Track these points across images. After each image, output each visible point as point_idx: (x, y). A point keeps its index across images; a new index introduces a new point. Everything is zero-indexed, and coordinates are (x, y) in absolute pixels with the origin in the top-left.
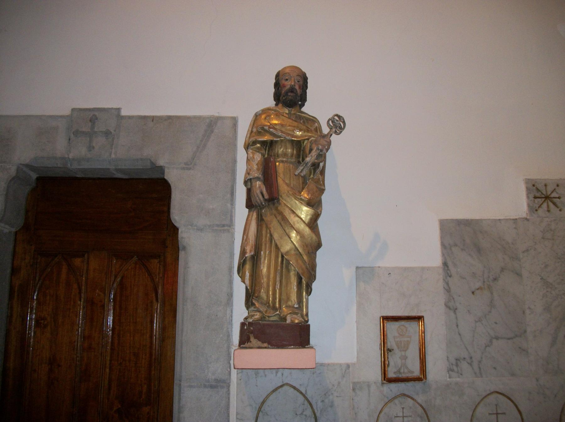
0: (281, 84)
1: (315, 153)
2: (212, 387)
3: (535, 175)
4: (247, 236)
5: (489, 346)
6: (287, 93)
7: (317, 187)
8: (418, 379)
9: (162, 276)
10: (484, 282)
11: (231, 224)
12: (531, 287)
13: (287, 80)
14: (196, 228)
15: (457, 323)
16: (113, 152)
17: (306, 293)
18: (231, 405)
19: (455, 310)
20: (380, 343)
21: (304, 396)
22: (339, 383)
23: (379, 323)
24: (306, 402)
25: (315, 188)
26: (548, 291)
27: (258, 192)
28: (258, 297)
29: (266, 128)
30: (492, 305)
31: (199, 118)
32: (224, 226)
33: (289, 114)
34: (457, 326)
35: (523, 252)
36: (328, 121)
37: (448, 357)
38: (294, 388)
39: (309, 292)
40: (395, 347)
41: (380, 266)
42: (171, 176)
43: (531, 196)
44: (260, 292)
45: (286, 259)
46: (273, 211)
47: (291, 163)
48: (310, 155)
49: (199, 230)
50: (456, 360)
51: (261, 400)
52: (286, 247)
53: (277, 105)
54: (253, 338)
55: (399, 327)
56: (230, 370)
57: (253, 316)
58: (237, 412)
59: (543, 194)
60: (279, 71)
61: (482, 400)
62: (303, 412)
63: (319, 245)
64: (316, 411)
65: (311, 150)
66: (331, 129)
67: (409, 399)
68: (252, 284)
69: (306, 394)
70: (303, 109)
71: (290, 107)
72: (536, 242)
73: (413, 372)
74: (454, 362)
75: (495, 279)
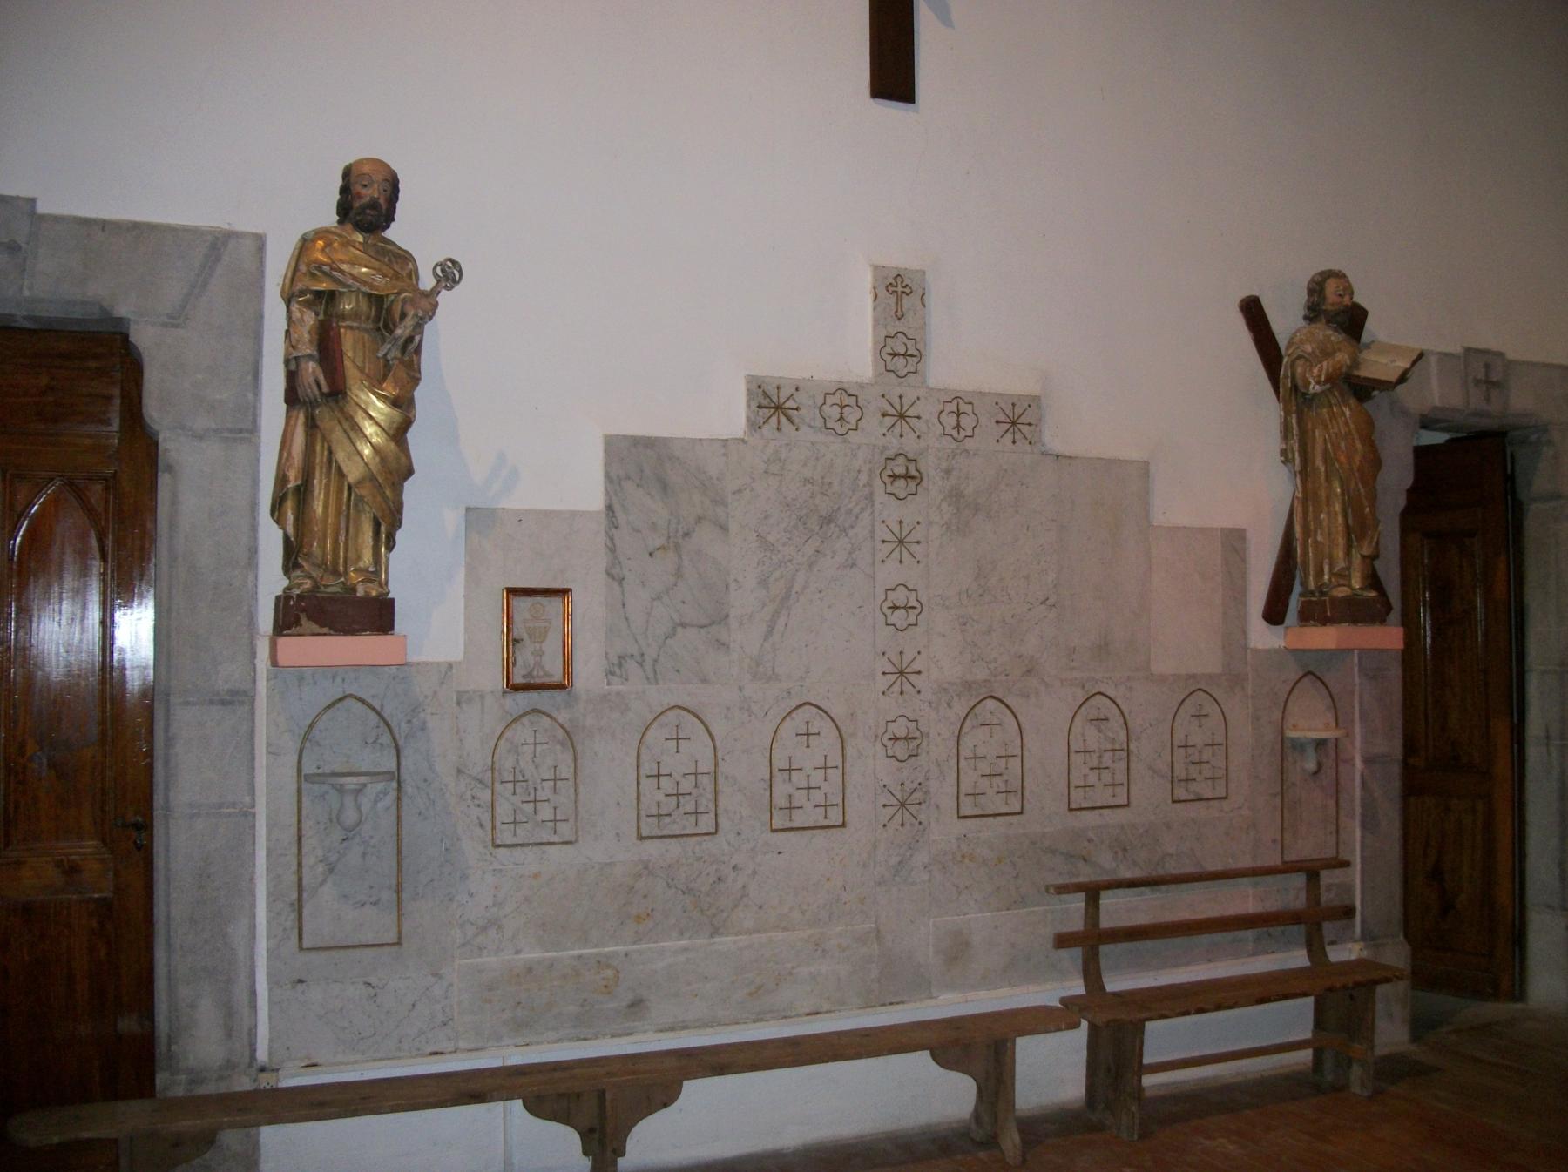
0: (353, 192)
1: (412, 323)
2: (223, 703)
3: (762, 371)
4: (289, 454)
5: (671, 638)
6: (363, 209)
7: (408, 374)
8: (561, 686)
10: (669, 537)
11: (254, 429)
12: (741, 548)
13: (365, 186)
14: (190, 433)
15: (623, 601)
16: (26, 283)
17: (386, 548)
18: (257, 731)
19: (621, 581)
20: (500, 630)
21: (378, 713)
22: (435, 693)
23: (500, 598)
24: (382, 724)
25: (405, 376)
26: (766, 556)
27: (311, 380)
28: (308, 555)
29: (326, 268)
30: (679, 573)
31: (195, 232)
32: (241, 431)
33: (365, 242)
34: (624, 605)
35: (734, 493)
36: (435, 268)
37: (606, 654)
38: (363, 701)
39: (390, 548)
40: (525, 636)
41: (506, 506)
42: (143, 337)
43: (754, 405)
44: (312, 546)
45: (356, 495)
46: (336, 413)
47: (366, 331)
48: (402, 326)
49: (196, 437)
50: (620, 657)
51: (308, 722)
52: (353, 473)
53: (340, 222)
54: (305, 619)
55: (533, 605)
56: (255, 674)
57: (300, 585)
58: (267, 743)
59: (773, 402)
60: (351, 164)
61: (656, 718)
62: (377, 739)
63: (410, 472)
64: (398, 737)
65: (403, 316)
66: (439, 281)
67: (545, 718)
68: (297, 533)
69: (382, 709)
70: (390, 234)
71: (366, 233)
72: (753, 479)
73: (551, 676)
74: (616, 661)
75: (686, 535)
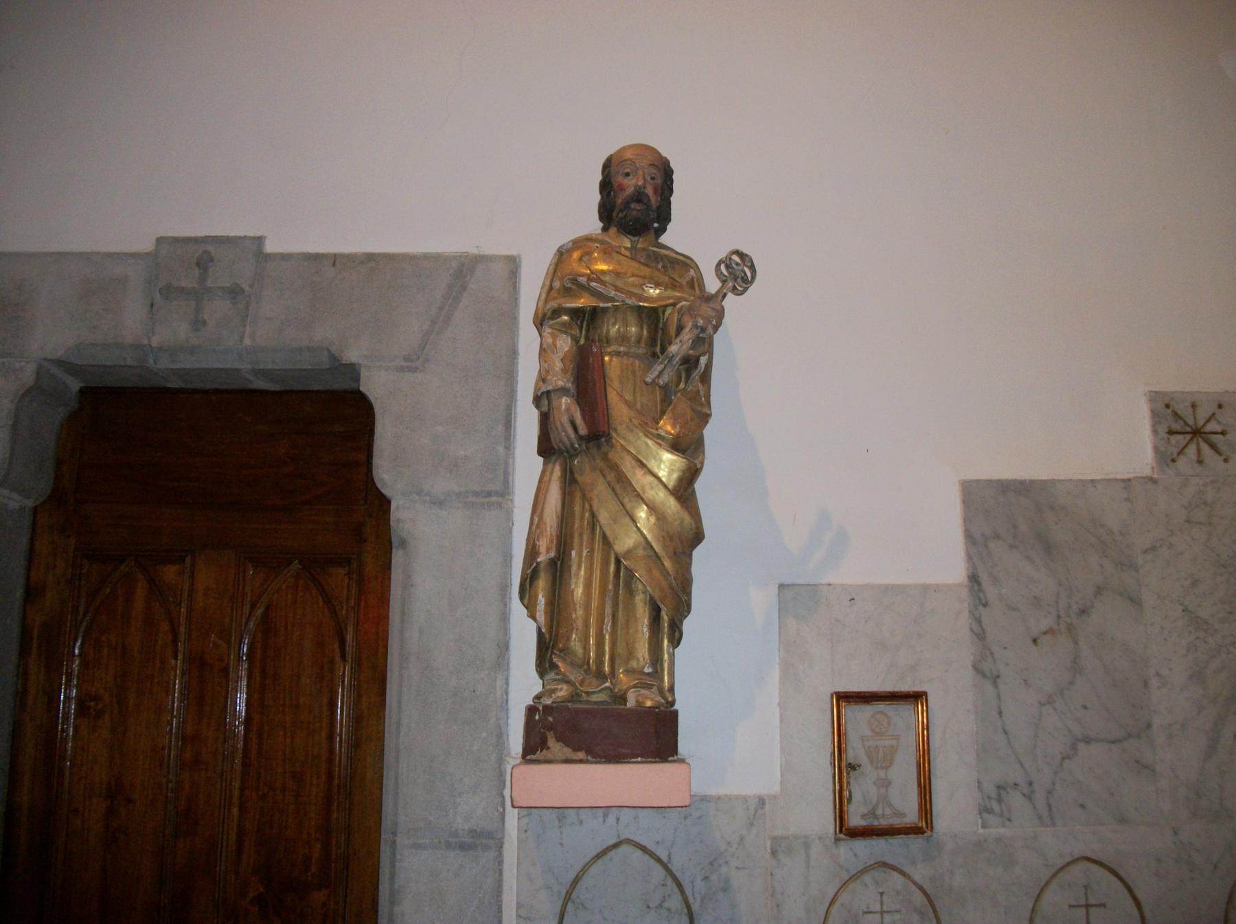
0: (615, 185)
1: (689, 336)
2: (463, 847)
3: (1170, 384)
4: (541, 517)
5: (1070, 758)
6: (627, 204)
7: (694, 410)
8: (915, 831)
10: (1059, 617)
11: (505, 491)
12: (1162, 628)
13: (627, 175)
14: (428, 498)
15: (999, 708)
16: (247, 332)
17: (669, 641)
18: (506, 887)
19: (995, 679)
20: (831, 750)
21: (665, 866)
22: (742, 839)
23: (829, 706)
24: (669, 881)
25: (689, 411)
26: (1198, 638)
27: (565, 419)
28: (565, 651)
29: (583, 280)
30: (1075, 667)
31: (436, 258)
32: (489, 494)
33: (633, 249)
34: (1000, 713)
35: (1145, 552)
36: (718, 265)
37: (979, 782)
38: (644, 849)
39: (676, 640)
40: (864, 760)
41: (832, 581)
42: (374, 385)
43: (1163, 429)
44: (568, 639)
45: (626, 568)
46: (598, 461)
47: (636, 356)
48: (678, 340)
49: (435, 503)
50: (999, 787)
51: (572, 875)
52: (625, 541)
53: (605, 229)
54: (554, 740)
55: (873, 716)
56: (504, 810)
57: (554, 691)
58: (518, 903)
59: (1188, 425)
60: (611, 156)
61: (1054, 876)
62: (663, 902)
63: (698, 537)
64: (691, 900)
65: (680, 329)
66: (724, 282)
67: (895, 874)
68: (552, 621)
69: (669, 862)
70: (664, 239)
71: (634, 235)
72: (1172, 531)
73: (903, 815)
74: (993, 792)
75: (1083, 612)
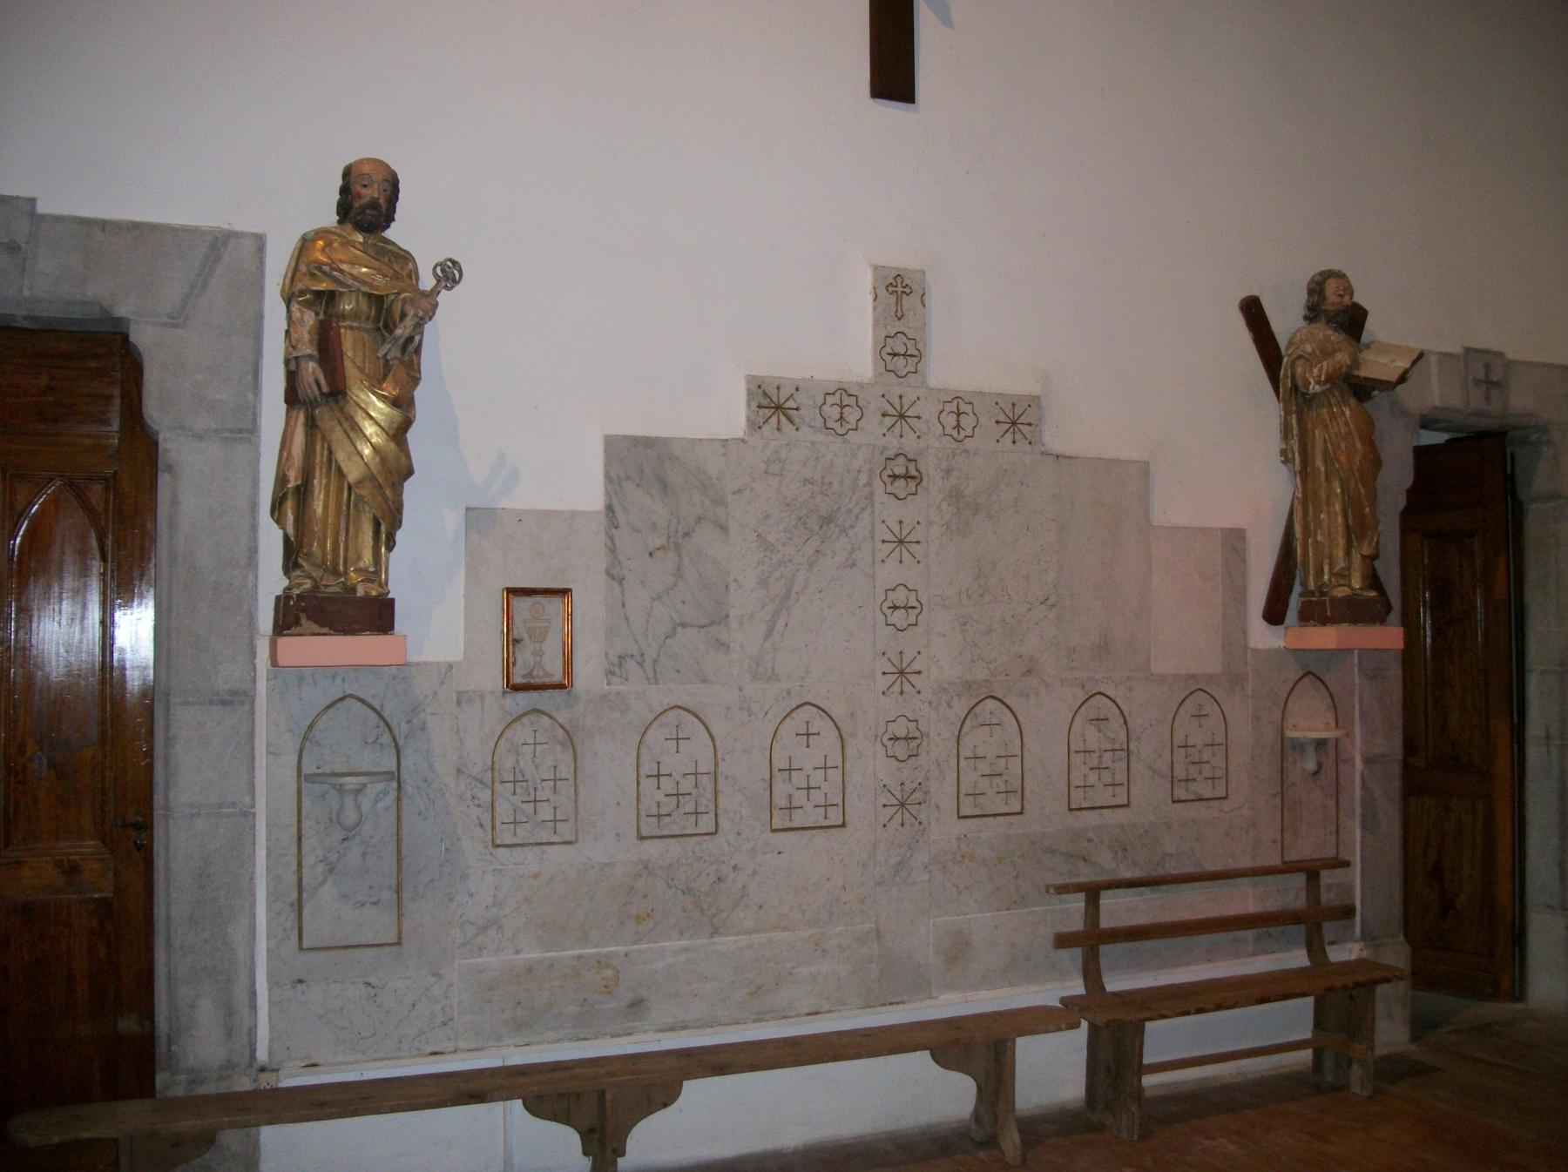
0: (353, 192)
1: (412, 323)
2: (223, 703)
3: (762, 371)
4: (289, 454)
5: (671, 638)
6: (363, 209)
7: (408, 374)
8: (561, 686)
9: (1314, 432)
10: (669, 537)
11: (254, 429)
12: (741, 548)
13: (365, 186)
14: (190, 433)
15: (623, 601)
16: (26, 283)
17: (386, 548)
18: (257, 731)
19: (621, 581)
20: (500, 630)
21: (378, 713)
22: (435, 693)
23: (500, 598)
24: (382, 724)
25: (405, 376)
26: (766, 556)
27: (311, 380)
28: (308, 555)
29: (326, 268)
30: (679, 573)
31: (195, 232)
32: (241, 431)
33: (365, 242)
34: (624, 605)
35: (734, 493)
36: (435, 268)
37: (606, 654)
38: (363, 701)
39: (390, 548)
40: (525, 636)
41: (506, 506)
42: (143, 337)
43: (754, 405)
44: (312, 546)
45: (356, 495)
46: (336, 413)
47: (366, 331)
48: (402, 326)
49: (196, 437)
50: (620, 657)
51: (308, 722)
52: (353, 473)
53: (340, 222)
54: (305, 619)
55: (533, 605)
56: (255, 674)
57: (300, 585)
58: (267, 743)
59: (773, 402)
60: (351, 164)
61: (656, 718)
62: (377, 739)
63: (410, 472)
64: (398, 737)
65: (403, 316)
66: (439, 281)
67: (545, 718)
68: (297, 533)
69: (382, 709)
70: (390, 234)
71: (366, 233)
72: (753, 479)
73: (551, 676)
74: (616, 661)
75: (686, 535)
